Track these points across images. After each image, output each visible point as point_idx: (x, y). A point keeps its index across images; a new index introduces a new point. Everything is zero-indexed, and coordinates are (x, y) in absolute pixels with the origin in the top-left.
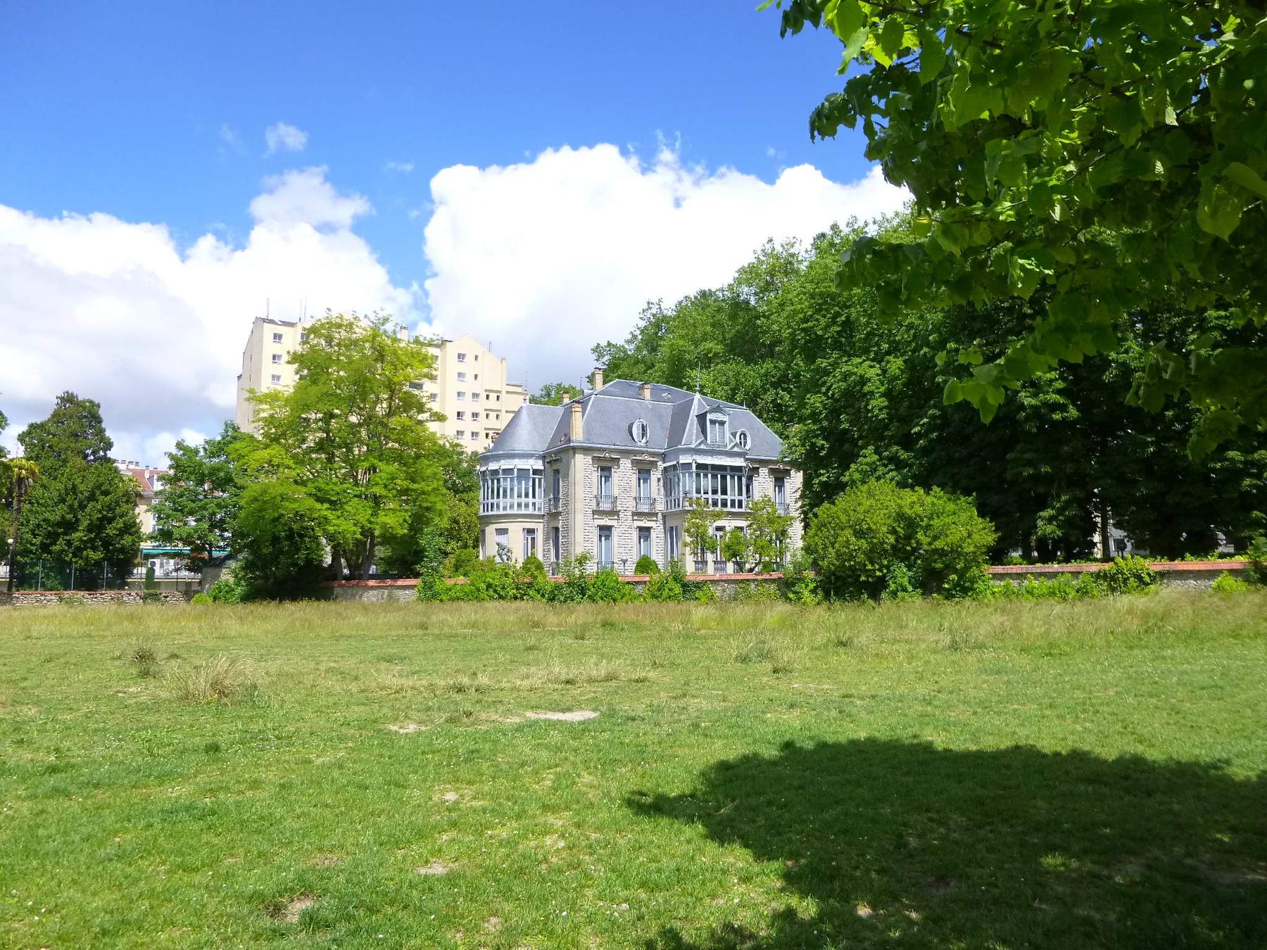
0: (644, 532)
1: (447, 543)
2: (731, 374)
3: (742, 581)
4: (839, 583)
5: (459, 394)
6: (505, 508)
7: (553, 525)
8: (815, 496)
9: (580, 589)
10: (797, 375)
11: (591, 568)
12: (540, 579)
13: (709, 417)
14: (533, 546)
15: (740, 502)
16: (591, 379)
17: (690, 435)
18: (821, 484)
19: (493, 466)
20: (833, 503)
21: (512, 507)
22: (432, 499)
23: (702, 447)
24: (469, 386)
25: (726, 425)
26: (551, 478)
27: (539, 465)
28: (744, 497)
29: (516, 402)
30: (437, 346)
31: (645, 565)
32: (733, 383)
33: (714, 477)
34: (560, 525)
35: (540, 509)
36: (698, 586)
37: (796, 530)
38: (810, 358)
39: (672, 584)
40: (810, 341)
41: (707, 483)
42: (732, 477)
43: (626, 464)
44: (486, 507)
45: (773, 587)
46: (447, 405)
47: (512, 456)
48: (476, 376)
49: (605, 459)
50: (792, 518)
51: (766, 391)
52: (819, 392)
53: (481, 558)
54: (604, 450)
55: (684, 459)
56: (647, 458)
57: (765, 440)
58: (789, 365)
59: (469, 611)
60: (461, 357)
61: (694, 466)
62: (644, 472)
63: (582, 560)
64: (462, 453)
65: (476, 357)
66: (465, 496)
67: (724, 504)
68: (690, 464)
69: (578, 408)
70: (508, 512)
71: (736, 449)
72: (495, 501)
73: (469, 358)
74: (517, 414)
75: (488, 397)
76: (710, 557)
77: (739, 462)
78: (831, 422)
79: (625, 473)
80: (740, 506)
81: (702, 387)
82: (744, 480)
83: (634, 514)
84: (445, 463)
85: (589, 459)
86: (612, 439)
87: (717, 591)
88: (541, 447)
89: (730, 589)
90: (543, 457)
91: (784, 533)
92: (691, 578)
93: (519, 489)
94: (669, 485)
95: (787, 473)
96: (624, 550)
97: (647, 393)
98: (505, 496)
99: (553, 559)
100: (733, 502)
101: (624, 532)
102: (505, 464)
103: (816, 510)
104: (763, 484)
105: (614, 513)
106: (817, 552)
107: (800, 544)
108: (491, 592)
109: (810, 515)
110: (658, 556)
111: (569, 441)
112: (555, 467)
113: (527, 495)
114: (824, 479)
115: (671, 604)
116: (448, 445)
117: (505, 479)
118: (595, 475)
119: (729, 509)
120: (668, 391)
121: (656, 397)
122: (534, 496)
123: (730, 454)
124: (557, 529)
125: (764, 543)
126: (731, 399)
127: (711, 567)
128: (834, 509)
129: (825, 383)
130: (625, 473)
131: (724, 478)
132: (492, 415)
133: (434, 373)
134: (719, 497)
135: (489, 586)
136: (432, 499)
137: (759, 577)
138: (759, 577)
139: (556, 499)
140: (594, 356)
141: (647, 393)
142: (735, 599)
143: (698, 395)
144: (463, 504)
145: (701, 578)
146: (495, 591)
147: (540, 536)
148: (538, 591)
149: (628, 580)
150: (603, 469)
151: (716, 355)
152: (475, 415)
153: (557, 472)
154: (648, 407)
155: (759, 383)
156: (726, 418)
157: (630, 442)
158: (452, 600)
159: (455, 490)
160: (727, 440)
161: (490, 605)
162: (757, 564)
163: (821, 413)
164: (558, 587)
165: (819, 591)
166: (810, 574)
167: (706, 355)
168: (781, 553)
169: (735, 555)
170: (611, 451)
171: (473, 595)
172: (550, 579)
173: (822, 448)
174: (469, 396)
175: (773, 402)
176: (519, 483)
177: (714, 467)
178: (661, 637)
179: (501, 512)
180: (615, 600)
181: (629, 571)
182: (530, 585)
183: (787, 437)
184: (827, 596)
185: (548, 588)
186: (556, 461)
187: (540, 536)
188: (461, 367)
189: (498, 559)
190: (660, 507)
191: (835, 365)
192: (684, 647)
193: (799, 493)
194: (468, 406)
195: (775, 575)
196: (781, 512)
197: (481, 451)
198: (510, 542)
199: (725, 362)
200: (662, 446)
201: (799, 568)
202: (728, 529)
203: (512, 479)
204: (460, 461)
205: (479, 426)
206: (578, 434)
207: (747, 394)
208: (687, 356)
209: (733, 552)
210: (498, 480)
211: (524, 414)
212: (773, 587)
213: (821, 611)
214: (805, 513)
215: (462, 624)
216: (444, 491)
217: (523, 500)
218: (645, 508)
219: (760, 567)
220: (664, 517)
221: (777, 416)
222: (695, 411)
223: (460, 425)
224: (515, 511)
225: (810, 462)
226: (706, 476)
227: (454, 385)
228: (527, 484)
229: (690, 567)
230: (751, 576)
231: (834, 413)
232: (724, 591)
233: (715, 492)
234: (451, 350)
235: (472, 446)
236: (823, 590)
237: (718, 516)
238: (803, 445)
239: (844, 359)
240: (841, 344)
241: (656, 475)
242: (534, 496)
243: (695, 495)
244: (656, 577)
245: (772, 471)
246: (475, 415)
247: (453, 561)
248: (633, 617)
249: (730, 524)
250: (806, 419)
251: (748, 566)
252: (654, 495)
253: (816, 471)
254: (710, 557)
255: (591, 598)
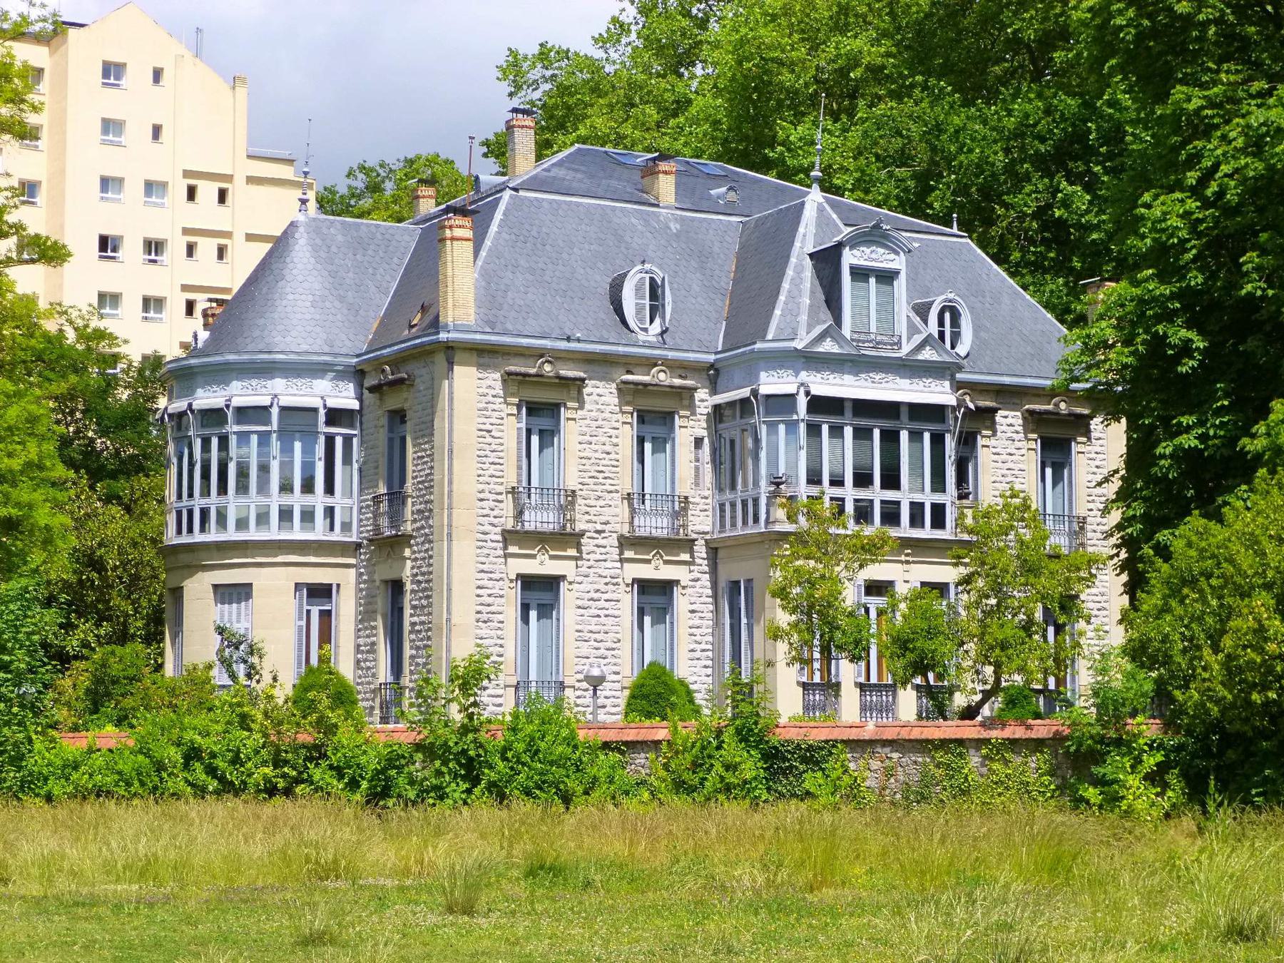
0: (654, 597)
1: (68, 626)
2: (915, 130)
3: (944, 744)
4: (1231, 755)
5: (105, 183)
6: (242, 524)
7: (385, 572)
8: (1164, 495)
9: (466, 765)
10: (1115, 136)
11: (498, 702)
12: (344, 735)
13: (850, 258)
14: (325, 636)
15: (938, 511)
16: (499, 149)
17: (792, 313)
18: (1182, 456)
19: (206, 398)
20: (1220, 520)
21: (263, 518)
22: (24, 493)
23: (828, 346)
24: (135, 160)
25: (901, 284)
26: (382, 436)
27: (345, 397)
28: (949, 497)
29: (274, 209)
30: (38, 38)
31: (655, 693)
32: (922, 155)
33: (862, 434)
34: (407, 572)
35: (346, 527)
36: (813, 756)
37: (1106, 594)
38: (1155, 84)
39: (732, 749)
40: (1154, 33)
41: (842, 452)
42: (916, 436)
43: (601, 395)
44: (185, 521)
45: (1033, 766)
46: (75, 218)
47: (266, 370)
48: (157, 131)
49: (538, 380)
50: (1092, 561)
51: (1019, 181)
52: (1178, 186)
53: (169, 670)
54: (539, 354)
55: (773, 383)
56: (663, 377)
57: (1017, 329)
58: (1088, 105)
59: (132, 829)
60: (112, 71)
61: (802, 402)
62: (654, 418)
63: (470, 679)
64: (116, 358)
65: (157, 75)
66: (122, 486)
67: (891, 515)
68: (792, 397)
69: (461, 228)
70: (253, 534)
71: (928, 354)
72: (198, 502)
73: (137, 76)
74: (280, 244)
75: (191, 193)
76: (847, 672)
77: (938, 393)
78: (1213, 276)
79: (598, 424)
80: (938, 522)
81: (827, 170)
82: (950, 444)
83: (626, 542)
84: (60, 387)
85: (494, 379)
86: (558, 321)
87: (868, 771)
88: (352, 343)
89: (909, 767)
90: (358, 374)
91: (1068, 603)
92: (793, 735)
93: (286, 467)
94: (728, 460)
95: (1081, 425)
96: (596, 649)
97: (666, 186)
98: (242, 488)
99: (384, 673)
100: (917, 509)
101: (597, 594)
102: (242, 393)
103: (1163, 536)
104: (1008, 458)
105: (565, 539)
106: (1167, 661)
107: (1118, 637)
108: (200, 774)
109: (1147, 550)
110: (694, 667)
111: (435, 325)
112: (393, 402)
113: (308, 487)
114: (1189, 441)
115: (733, 810)
116: (71, 335)
117: (243, 437)
118: (511, 426)
119: (905, 530)
120: (730, 184)
121: (691, 197)
122: (329, 489)
123: (911, 368)
124: (396, 587)
125: (1009, 632)
126: (915, 205)
127: (849, 704)
128: (1218, 533)
129: (1196, 158)
130: (598, 424)
131: (890, 438)
132: (207, 247)
133: (32, 119)
134: (877, 494)
135: (192, 754)
136: (24, 493)
137: (995, 734)
138: (995, 734)
139: (396, 497)
140: (506, 87)
141: (666, 186)
142: (923, 798)
143: (815, 196)
144: (116, 510)
145: (822, 735)
146: (211, 771)
147: (346, 607)
148: (339, 771)
149: (611, 736)
150: (534, 409)
151: (875, 72)
152: (154, 247)
153: (398, 417)
154: (662, 242)
155: (1000, 159)
156: (897, 262)
157: (612, 331)
158: (82, 795)
159: (89, 465)
160: (902, 328)
161: (193, 808)
162: (987, 695)
163: (1182, 246)
164: (393, 761)
165: (1173, 777)
166: (1146, 728)
167: (843, 73)
168: (1061, 664)
169: (920, 667)
170: (557, 357)
171: (148, 782)
172: (376, 735)
173: (1185, 349)
174: (134, 189)
175: (1041, 213)
176: (287, 450)
177: (864, 408)
178: (699, 907)
179: (232, 535)
180: (567, 799)
181: (610, 712)
182: (316, 753)
183: (1081, 320)
184: (1196, 792)
185: (371, 762)
186: (396, 385)
187: (346, 607)
188: (112, 103)
189: (219, 676)
190: (701, 522)
191: (1228, 106)
192: (768, 936)
193: (1116, 484)
194: (132, 219)
195: (1041, 729)
196: (1059, 541)
197: (171, 351)
198: (258, 623)
199: (898, 96)
200: (706, 343)
201: (1112, 708)
202: (901, 589)
203: (264, 438)
204: (110, 384)
205: (168, 279)
206: (462, 306)
207: (962, 190)
208: (786, 77)
209: (917, 659)
210: (224, 441)
211: (301, 252)
212: (1033, 766)
213: (1180, 837)
214: (1128, 543)
215: (108, 869)
216: (60, 471)
217: (297, 500)
218: (654, 525)
219: (998, 702)
220: (714, 552)
221: (1052, 257)
222: (806, 240)
223: (109, 276)
224: (273, 533)
225: (1148, 395)
226: (836, 431)
227: (89, 158)
228: (308, 451)
229: (786, 699)
230: (969, 730)
231: (1222, 247)
232: (889, 773)
233: (863, 479)
234: (83, 54)
235: (144, 338)
236: (1184, 775)
237: (871, 550)
238: (1128, 342)
239: (1258, 85)
240: (1246, 42)
241: (690, 429)
242: (329, 489)
243: (803, 490)
244: (687, 731)
245: (1034, 421)
246: (154, 247)
247: (85, 681)
248: (617, 848)
249: (907, 576)
250: (1137, 267)
251: (960, 700)
252: (684, 488)
253: (1166, 421)
254: (847, 672)
255: (499, 793)
